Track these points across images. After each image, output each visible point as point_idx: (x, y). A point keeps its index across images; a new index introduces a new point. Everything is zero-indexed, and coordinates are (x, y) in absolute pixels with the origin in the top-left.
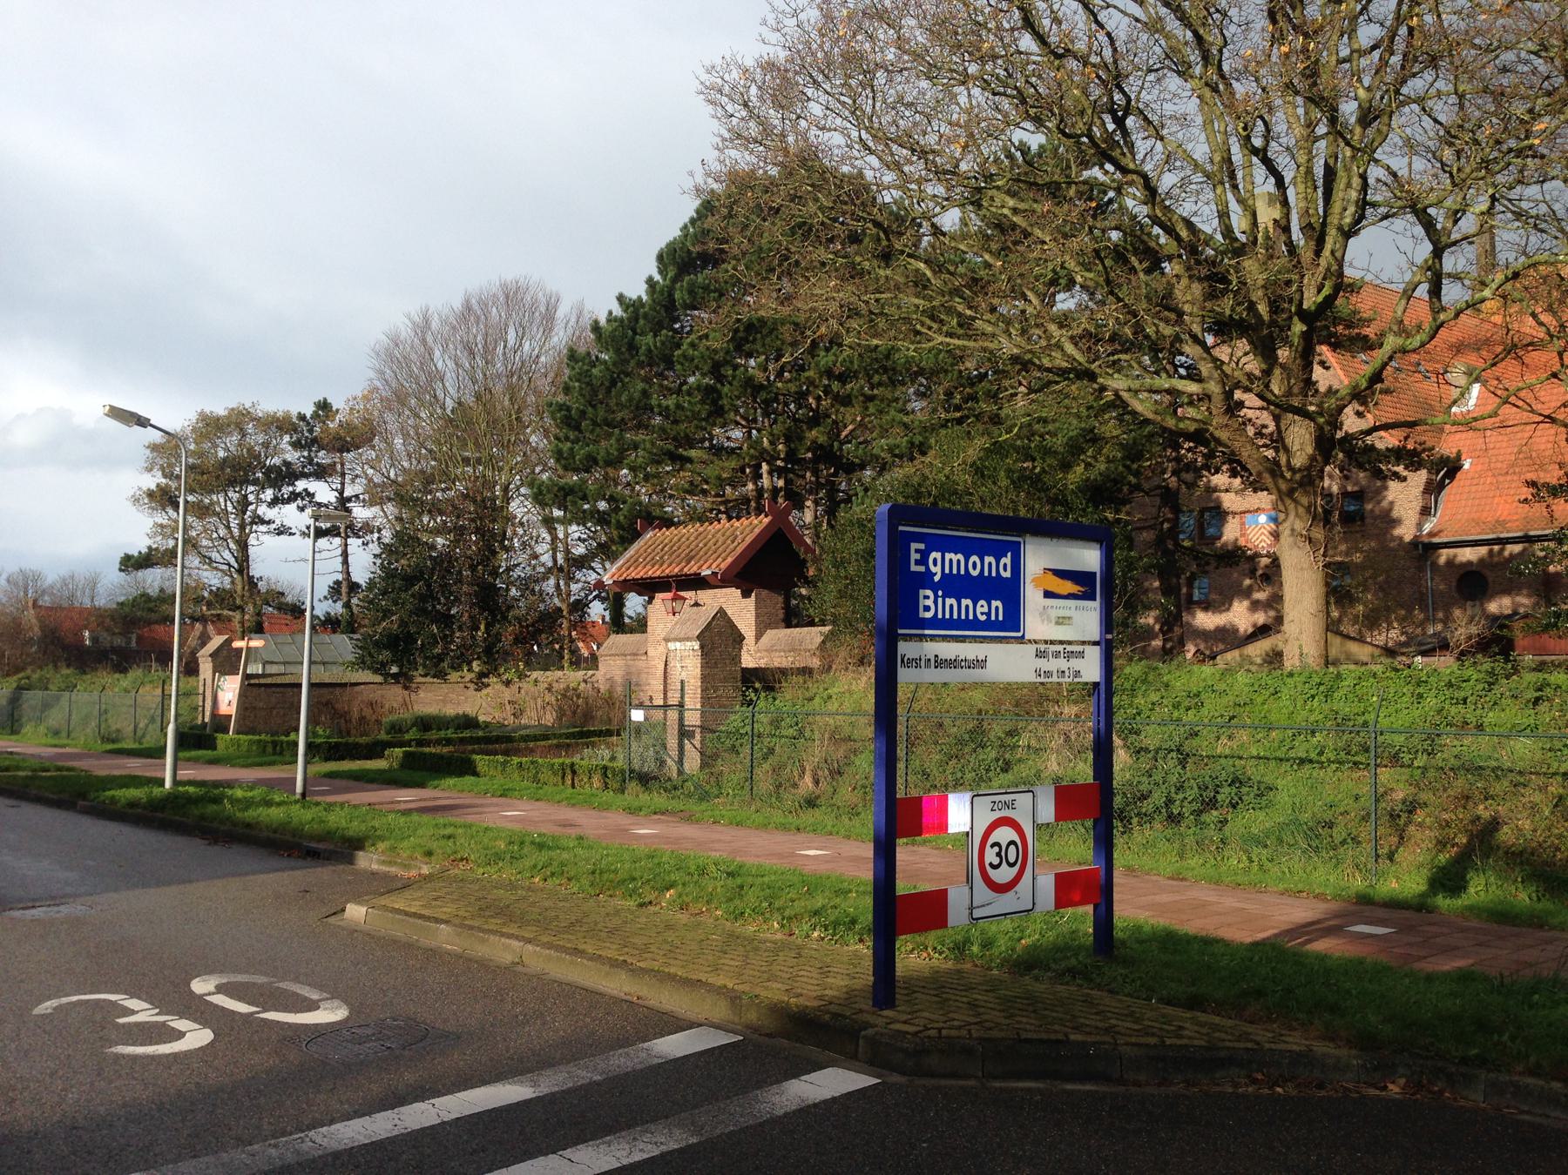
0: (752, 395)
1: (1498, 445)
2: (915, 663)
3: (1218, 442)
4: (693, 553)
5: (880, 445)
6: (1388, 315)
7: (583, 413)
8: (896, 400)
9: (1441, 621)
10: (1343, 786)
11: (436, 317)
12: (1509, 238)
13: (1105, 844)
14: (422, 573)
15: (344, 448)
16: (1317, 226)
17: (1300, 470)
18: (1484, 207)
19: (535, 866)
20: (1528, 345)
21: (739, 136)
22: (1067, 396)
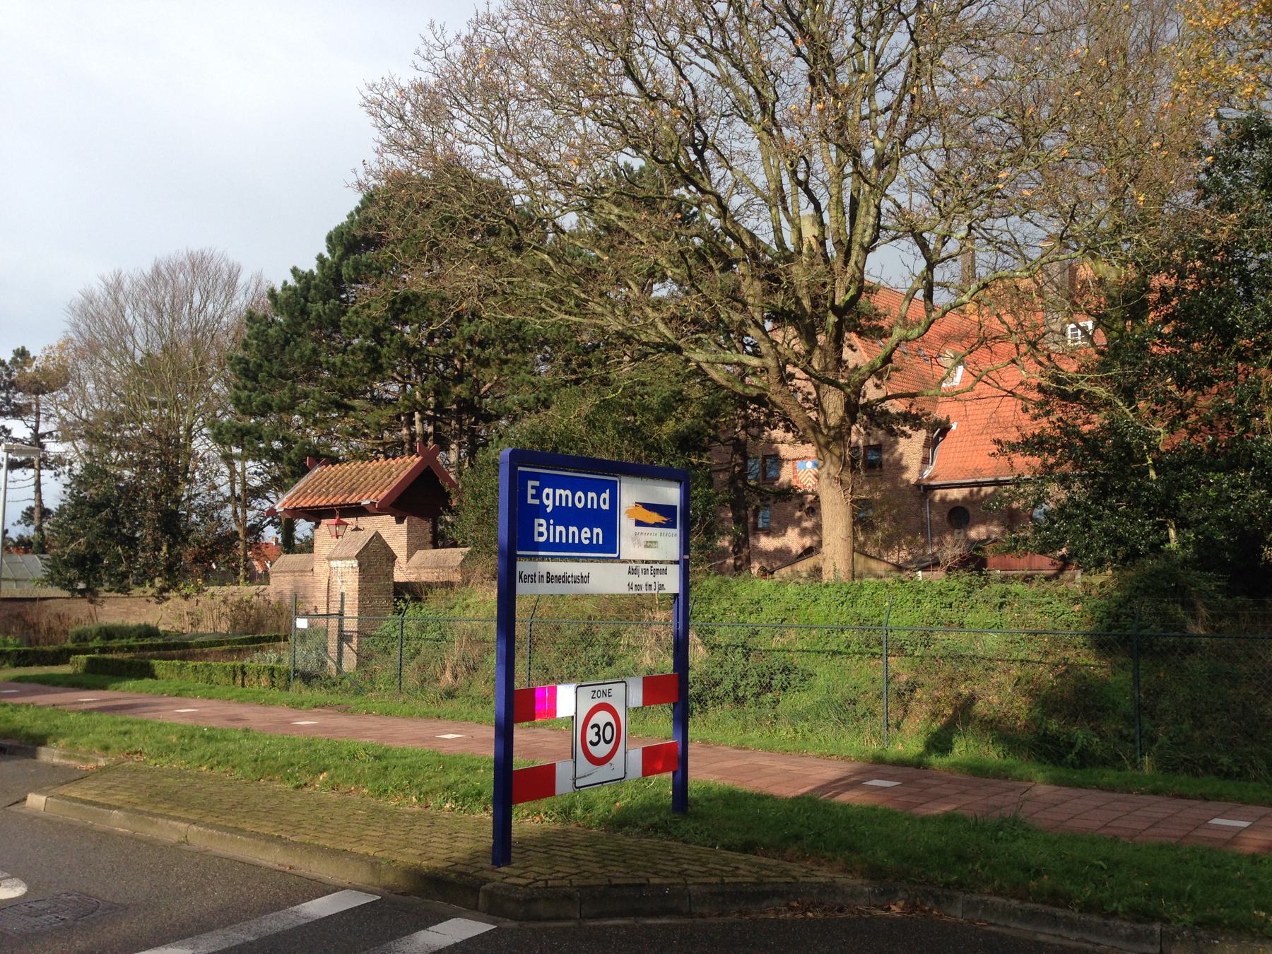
0: (407, 356)
1: (976, 412)
2: (531, 578)
3: (774, 404)
4: (355, 486)
5: (512, 400)
6: (895, 312)
7: (260, 366)
8: (526, 364)
9: (938, 544)
10: (864, 672)
11: (128, 280)
12: (985, 256)
13: (682, 720)
14: (109, 500)
15: (39, 390)
16: (845, 242)
17: (834, 428)
18: (963, 234)
19: (203, 756)
20: (995, 338)
21: (396, 143)
22: (661, 364)
